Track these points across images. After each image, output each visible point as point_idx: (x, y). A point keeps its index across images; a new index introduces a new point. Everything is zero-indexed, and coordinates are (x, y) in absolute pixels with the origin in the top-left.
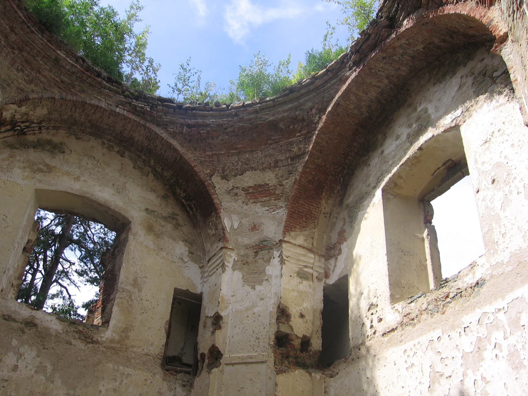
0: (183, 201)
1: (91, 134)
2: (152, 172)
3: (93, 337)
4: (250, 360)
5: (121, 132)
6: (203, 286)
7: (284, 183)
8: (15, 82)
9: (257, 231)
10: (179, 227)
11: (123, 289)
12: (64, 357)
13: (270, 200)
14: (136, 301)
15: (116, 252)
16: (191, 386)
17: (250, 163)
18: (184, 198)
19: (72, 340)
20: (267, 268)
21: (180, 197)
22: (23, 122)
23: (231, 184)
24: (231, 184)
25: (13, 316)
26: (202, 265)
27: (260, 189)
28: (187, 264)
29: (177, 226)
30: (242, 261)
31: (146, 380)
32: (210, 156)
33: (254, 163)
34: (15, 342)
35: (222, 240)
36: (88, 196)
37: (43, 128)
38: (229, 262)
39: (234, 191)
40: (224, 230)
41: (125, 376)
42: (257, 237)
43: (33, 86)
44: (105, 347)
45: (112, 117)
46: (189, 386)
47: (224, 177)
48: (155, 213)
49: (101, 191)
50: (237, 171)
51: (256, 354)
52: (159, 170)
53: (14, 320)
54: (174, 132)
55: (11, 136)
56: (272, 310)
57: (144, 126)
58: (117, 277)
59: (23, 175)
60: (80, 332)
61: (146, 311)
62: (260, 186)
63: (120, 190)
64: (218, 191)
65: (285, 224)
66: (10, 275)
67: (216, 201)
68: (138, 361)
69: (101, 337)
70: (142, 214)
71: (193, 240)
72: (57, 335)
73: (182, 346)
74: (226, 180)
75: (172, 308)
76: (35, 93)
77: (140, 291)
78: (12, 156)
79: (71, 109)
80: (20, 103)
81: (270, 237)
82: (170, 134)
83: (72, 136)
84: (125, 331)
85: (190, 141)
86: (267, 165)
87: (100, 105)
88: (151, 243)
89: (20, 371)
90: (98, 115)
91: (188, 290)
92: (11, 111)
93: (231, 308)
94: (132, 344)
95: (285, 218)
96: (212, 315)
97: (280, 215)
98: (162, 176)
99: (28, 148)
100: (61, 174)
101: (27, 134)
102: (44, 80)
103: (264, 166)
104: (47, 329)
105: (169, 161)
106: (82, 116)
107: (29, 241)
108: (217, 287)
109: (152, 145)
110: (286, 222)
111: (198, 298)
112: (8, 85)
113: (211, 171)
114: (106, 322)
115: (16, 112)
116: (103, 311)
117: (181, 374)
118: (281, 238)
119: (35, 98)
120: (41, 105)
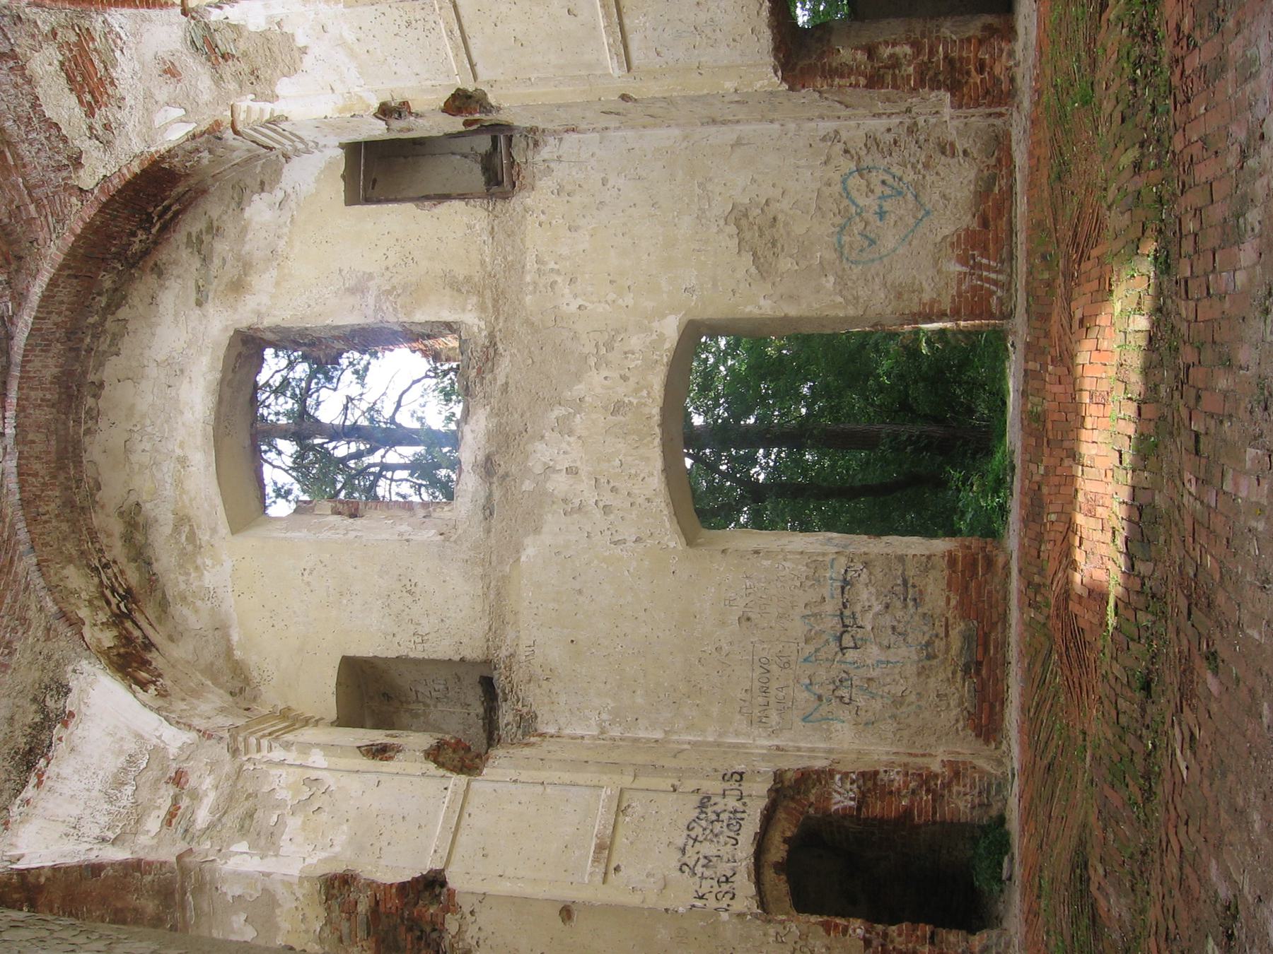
0: (154, 231)
1: (78, 463)
2: (113, 314)
3: (483, 346)
4: (457, 33)
5: (53, 406)
6: (325, 146)
7: (46, 29)
8: (37, 649)
9: (177, 64)
10: (215, 224)
11: (376, 311)
12: (533, 391)
13: (95, 50)
14: (393, 280)
15: (306, 341)
16: (533, 130)
17: (24, 114)
18: (148, 230)
19: (499, 383)
20: (252, 28)
21: (148, 239)
22: (108, 603)
23: (87, 145)
24: (87, 145)
25: (482, 501)
26: (281, 156)
27: (79, 79)
28: (289, 191)
29: (213, 229)
30: (252, 83)
31: (540, 225)
32: (39, 206)
33: (20, 105)
34: (528, 485)
35: (219, 135)
36: (210, 429)
37: (104, 560)
38: (262, 111)
39: (100, 133)
40: (194, 135)
41: (543, 268)
42: (190, 61)
43: (31, 613)
44: (496, 319)
45: (30, 437)
46: (534, 136)
47: (76, 161)
48: (200, 284)
49: (191, 408)
50: (53, 138)
51: (441, 22)
52: (103, 301)
53: (489, 497)
54: (13, 298)
55: (143, 613)
56: (341, 5)
57: (23, 367)
58: (356, 327)
59: (213, 566)
60: (480, 372)
61: (408, 255)
62: (70, 79)
63: (178, 371)
64: (112, 169)
65: (143, 7)
66: (410, 529)
67: (136, 168)
68: (508, 249)
69: (480, 330)
70: (211, 311)
71: (233, 187)
72: (496, 413)
73: (458, 157)
74: (80, 157)
75: (388, 201)
76: (43, 604)
77: (370, 276)
78: (184, 599)
79: (46, 522)
80: (76, 624)
81: (181, 33)
82: (20, 305)
83: (97, 499)
84: (456, 286)
85: (20, 258)
86: (16, 75)
87: (15, 470)
88: (266, 276)
89: (575, 461)
90: (37, 466)
91: (343, 177)
92: (99, 635)
93: (357, 89)
94: (478, 268)
95: (127, 11)
96: (384, 123)
97: (122, 20)
98: (116, 290)
99: (154, 574)
100: (184, 496)
101: (128, 586)
102: (9, 597)
103: (20, 81)
104: (490, 436)
105: (79, 288)
106: (49, 496)
107: (336, 512)
108: (323, 124)
109: (58, 335)
110: (137, 7)
111: (354, 151)
112: (49, 658)
113: (71, 195)
114: (450, 327)
115: (95, 625)
116: (429, 337)
117: (514, 154)
118: (179, 10)
119: (54, 600)
120: (61, 584)
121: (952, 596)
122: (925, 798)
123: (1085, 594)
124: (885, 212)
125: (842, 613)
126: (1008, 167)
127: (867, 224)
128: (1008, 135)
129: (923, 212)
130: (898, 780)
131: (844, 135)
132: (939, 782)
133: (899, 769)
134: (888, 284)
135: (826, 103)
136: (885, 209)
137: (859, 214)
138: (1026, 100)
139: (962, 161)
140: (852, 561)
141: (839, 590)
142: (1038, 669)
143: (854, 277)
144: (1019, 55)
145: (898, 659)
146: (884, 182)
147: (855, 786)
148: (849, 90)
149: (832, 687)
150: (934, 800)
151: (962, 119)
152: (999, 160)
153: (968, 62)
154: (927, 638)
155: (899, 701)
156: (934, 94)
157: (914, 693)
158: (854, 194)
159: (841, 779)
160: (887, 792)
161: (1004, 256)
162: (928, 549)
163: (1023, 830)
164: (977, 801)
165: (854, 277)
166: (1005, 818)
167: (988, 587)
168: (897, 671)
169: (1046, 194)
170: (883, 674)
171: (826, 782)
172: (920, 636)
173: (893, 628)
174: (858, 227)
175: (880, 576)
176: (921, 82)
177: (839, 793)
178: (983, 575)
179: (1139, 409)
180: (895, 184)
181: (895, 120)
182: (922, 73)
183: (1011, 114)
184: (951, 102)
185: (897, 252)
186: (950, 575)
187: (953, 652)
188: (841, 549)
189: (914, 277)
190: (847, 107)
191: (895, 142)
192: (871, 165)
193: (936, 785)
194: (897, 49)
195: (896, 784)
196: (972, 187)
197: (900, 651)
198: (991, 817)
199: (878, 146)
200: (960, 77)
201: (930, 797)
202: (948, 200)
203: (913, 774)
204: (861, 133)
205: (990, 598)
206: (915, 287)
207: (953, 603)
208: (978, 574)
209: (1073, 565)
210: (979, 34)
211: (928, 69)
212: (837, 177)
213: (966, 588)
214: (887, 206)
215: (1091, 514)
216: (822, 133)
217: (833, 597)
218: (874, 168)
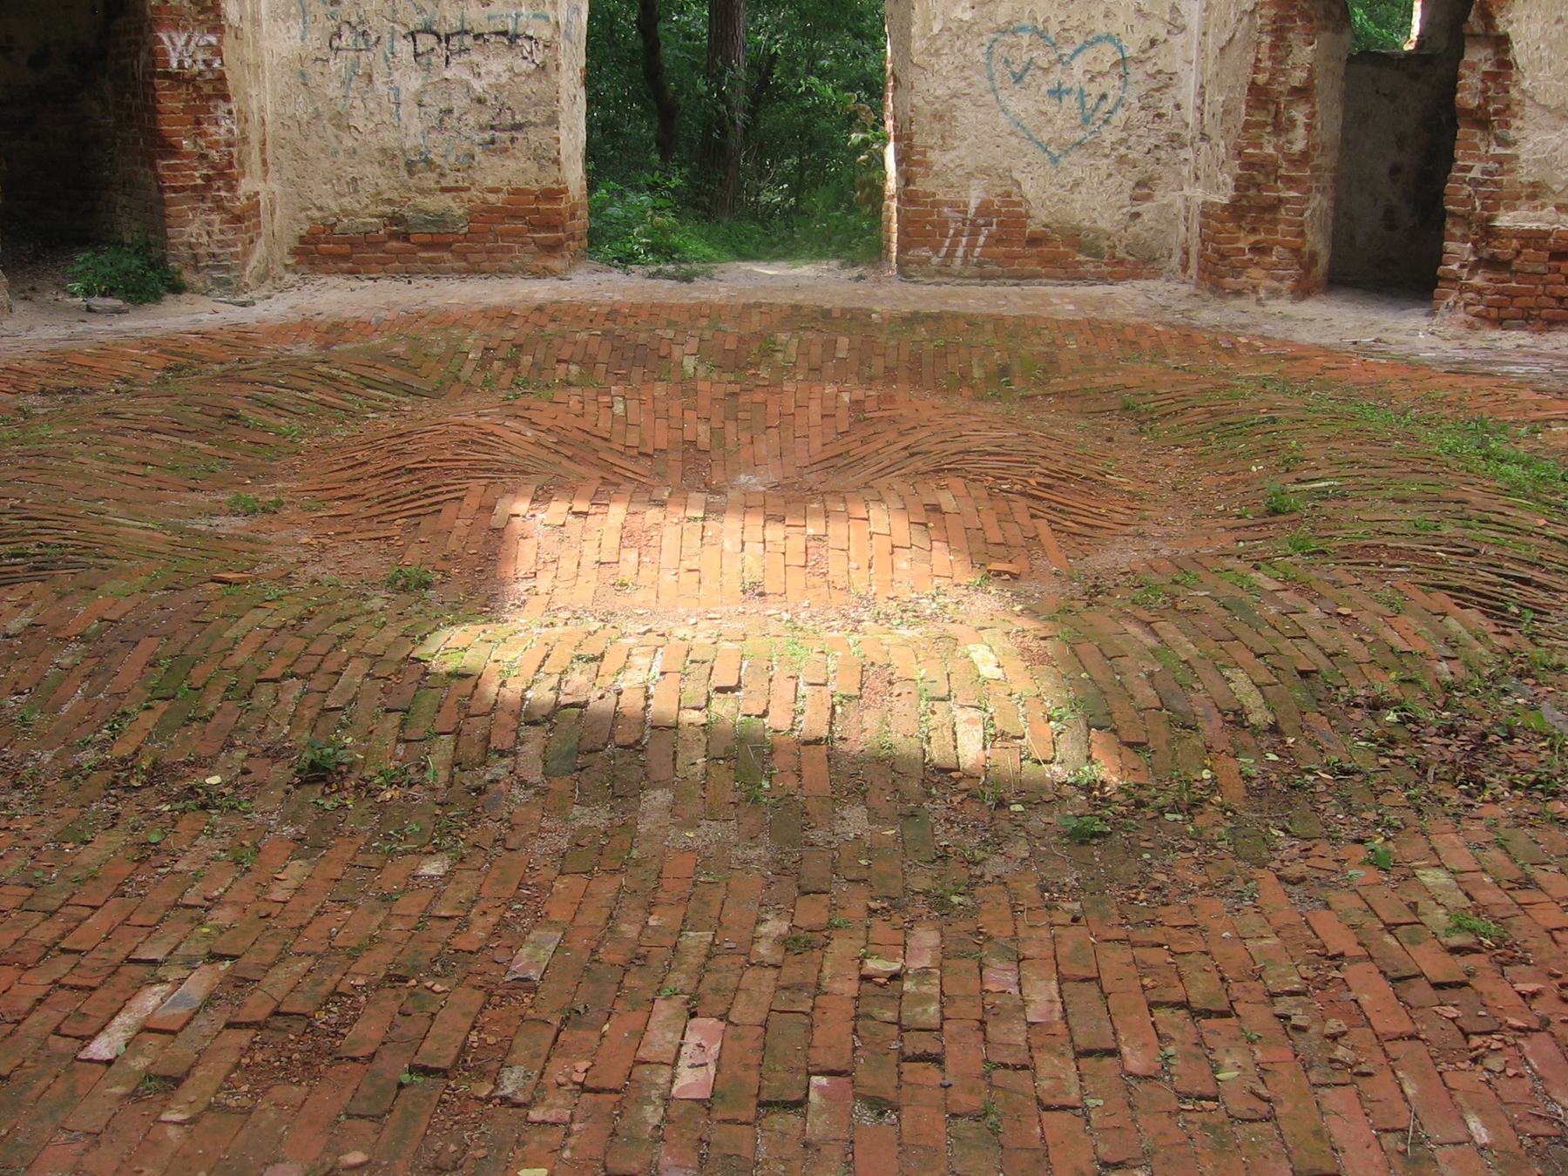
121: (501, 195)
122: (197, 174)
123: (496, 521)
124: (1060, 99)
125: (466, 32)
126: (1111, 274)
127: (1045, 71)
128: (1155, 275)
129: (1056, 153)
130: (220, 132)
131: (1177, 40)
132: (223, 194)
133: (236, 132)
134: (955, 101)
135: (1232, 19)
136: (1065, 98)
137: (1060, 58)
138: (1210, 315)
139: (1125, 210)
140: (545, 46)
141: (501, 28)
142: (391, 374)
143: (968, 50)
144: (1275, 306)
145: (404, 119)
146: (1104, 97)
147: (202, 67)
148: (1251, 58)
149: (354, 19)
150: (195, 188)
151: (1183, 213)
152: (1121, 262)
153: (1268, 232)
154: (438, 160)
155: (341, 122)
156: (1229, 180)
157: (356, 144)
158: (1090, 53)
159: (210, 45)
160: (198, 119)
161: (988, 268)
162: (568, 158)
163: (151, 346)
164: (201, 251)
165: (968, 50)
166: (180, 293)
167: (517, 247)
168: (386, 118)
169: (1099, 380)
170: (380, 97)
171: (202, 22)
172: (441, 151)
173: (450, 111)
174: (1042, 57)
175: (526, 89)
176: (1248, 164)
177: (187, 43)
178: (534, 240)
179: (818, 741)
180: (1099, 114)
181: (1191, 117)
182: (1263, 166)
183: (1184, 283)
184: (1213, 204)
185: (1001, 115)
186: (532, 193)
187: (419, 199)
188: (563, 29)
189: (965, 139)
190: (1222, 49)
191: (1159, 116)
192: (1131, 79)
193: (219, 189)
194: (1300, 131)
195: (213, 129)
196: (1087, 224)
197: (416, 121)
198: (179, 273)
199: (1158, 90)
200: (1249, 219)
201: (199, 181)
202: (1071, 190)
203: (231, 154)
204: (1178, 66)
205: (502, 249)
206: (949, 140)
207: (492, 198)
208: (535, 232)
209: (542, 496)
210: (1306, 249)
211: (1267, 175)
212: (1117, 27)
213: (514, 216)
214: (1070, 102)
215: (627, 537)
216: (1183, 9)
217: (489, 18)
218: (1126, 83)
